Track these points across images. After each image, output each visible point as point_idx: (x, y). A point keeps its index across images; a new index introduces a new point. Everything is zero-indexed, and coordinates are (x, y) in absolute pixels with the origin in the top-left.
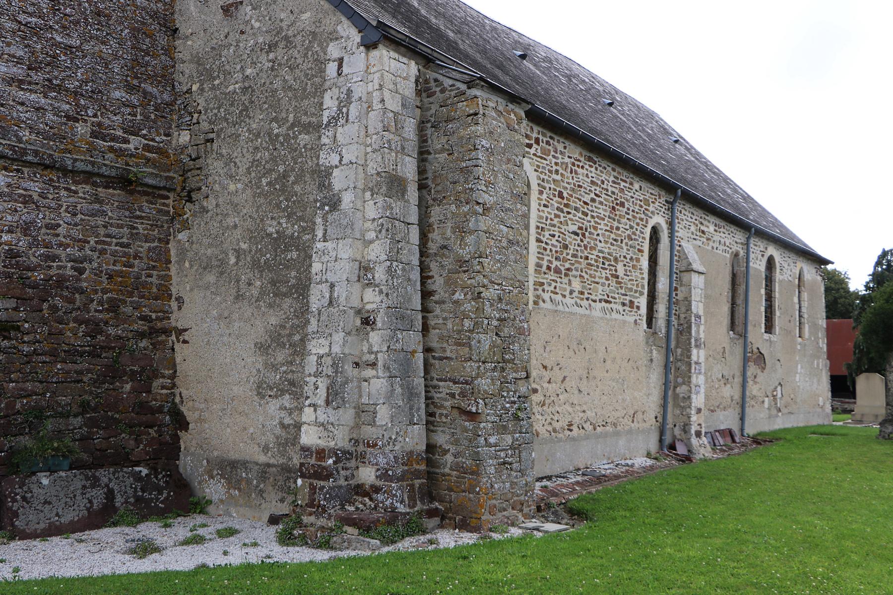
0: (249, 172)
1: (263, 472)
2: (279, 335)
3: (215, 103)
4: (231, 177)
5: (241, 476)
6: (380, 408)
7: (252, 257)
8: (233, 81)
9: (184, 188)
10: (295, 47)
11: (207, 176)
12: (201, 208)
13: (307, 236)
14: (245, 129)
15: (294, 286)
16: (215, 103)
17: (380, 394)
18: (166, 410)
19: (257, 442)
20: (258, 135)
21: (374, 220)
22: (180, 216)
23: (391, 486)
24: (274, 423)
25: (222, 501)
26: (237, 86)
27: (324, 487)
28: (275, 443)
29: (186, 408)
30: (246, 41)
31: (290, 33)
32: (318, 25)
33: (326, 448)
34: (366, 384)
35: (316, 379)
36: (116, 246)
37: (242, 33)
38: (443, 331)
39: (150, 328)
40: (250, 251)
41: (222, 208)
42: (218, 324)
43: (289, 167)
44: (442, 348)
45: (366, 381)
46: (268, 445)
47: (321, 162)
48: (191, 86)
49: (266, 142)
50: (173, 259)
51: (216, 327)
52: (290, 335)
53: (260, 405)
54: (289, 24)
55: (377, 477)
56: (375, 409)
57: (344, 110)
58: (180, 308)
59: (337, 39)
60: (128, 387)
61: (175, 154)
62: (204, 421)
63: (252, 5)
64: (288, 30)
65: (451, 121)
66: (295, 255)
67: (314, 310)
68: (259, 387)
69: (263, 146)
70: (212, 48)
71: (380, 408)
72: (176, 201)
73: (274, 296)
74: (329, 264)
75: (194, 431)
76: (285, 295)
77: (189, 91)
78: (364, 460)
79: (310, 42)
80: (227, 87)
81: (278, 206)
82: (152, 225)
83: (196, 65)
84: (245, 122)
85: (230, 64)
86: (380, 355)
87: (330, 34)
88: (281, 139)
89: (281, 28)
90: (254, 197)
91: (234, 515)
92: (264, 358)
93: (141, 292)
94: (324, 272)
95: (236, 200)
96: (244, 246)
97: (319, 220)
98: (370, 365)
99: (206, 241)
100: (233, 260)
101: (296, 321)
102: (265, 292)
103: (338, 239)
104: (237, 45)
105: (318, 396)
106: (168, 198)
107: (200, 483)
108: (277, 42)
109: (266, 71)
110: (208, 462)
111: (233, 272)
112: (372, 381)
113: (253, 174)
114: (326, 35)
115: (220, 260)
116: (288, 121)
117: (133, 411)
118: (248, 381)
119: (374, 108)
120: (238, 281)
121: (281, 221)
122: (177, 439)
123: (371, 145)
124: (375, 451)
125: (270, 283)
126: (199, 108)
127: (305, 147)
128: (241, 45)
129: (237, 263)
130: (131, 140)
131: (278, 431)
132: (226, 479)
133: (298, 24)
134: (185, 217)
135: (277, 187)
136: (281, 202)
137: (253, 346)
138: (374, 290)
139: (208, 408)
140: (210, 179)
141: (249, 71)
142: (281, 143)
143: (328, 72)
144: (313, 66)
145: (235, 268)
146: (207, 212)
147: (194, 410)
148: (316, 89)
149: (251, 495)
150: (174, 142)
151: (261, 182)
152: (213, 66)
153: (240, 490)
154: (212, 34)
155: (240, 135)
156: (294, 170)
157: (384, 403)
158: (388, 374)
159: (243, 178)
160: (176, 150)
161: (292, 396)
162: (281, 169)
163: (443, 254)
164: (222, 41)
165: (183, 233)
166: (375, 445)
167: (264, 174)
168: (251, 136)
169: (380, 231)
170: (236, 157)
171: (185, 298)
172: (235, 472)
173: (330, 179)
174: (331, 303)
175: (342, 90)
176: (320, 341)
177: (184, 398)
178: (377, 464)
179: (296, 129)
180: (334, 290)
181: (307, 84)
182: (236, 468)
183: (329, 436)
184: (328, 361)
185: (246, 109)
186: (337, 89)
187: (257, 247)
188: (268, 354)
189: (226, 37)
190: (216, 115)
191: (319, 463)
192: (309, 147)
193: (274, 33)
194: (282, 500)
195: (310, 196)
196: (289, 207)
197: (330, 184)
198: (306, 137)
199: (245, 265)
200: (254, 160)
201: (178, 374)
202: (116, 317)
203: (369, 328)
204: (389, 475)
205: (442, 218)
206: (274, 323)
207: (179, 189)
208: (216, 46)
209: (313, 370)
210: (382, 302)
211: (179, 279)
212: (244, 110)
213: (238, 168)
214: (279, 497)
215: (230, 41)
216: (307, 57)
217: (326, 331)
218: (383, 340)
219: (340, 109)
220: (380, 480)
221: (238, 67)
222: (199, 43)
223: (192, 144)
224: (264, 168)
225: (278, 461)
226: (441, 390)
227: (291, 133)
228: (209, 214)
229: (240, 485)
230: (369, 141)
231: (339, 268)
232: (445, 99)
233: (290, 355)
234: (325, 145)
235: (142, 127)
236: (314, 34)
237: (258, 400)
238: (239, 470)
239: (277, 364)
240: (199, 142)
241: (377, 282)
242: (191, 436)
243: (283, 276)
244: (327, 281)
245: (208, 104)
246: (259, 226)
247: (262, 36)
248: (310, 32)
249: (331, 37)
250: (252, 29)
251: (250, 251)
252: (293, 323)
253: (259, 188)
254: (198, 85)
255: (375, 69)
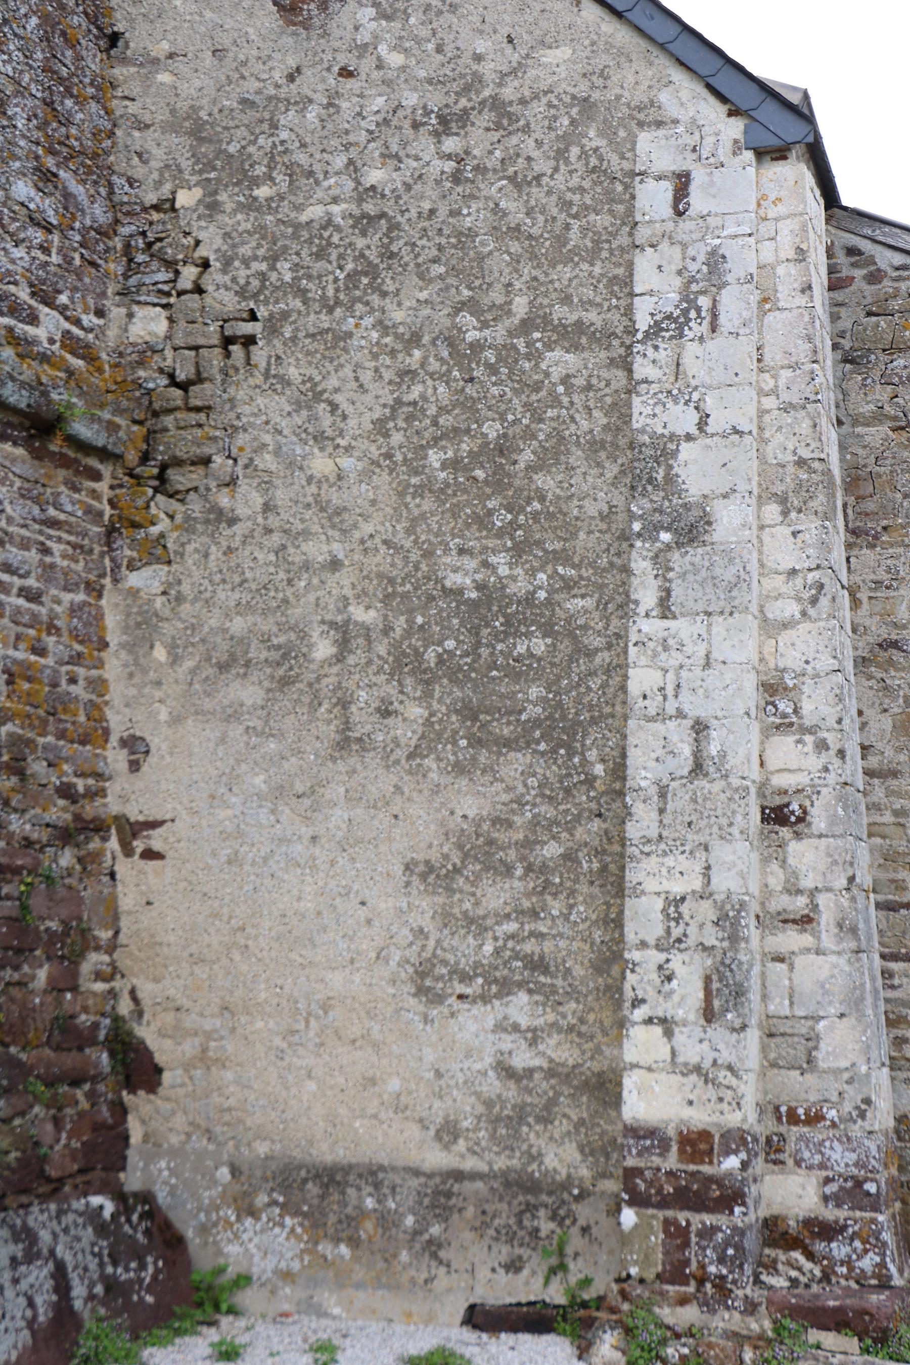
0: (381, 427)
1: (437, 1193)
2: (491, 842)
3: (259, 246)
4: (320, 438)
5: (359, 1208)
6: (831, 1028)
7: (396, 645)
8: (320, 194)
9: (145, 458)
10: (526, 129)
11: (232, 430)
12: (210, 511)
13: (580, 603)
14: (368, 321)
15: (536, 723)
16: (259, 246)
17: (826, 993)
18: (102, 1035)
19: (416, 1115)
20: (414, 340)
21: (793, 572)
22: (135, 525)
23: (873, 1221)
24: (478, 1066)
25: (287, 1276)
26: (336, 209)
27: (715, 1229)
28: (479, 1118)
29: (153, 1028)
30: (361, 96)
31: (508, 93)
32: (599, 82)
33: (713, 1130)
34: (782, 967)
35: (662, 957)
36: (19, 596)
37: (346, 73)
38: (894, 843)
39: (77, 817)
40: (387, 630)
41: (284, 516)
42: (273, 812)
43: (517, 429)
44: (893, 881)
45: (782, 960)
46: (456, 1122)
47: (637, 423)
48: (174, 193)
49: (442, 360)
50: (114, 638)
51: (264, 816)
52: (528, 844)
53: (426, 1019)
54: (505, 69)
55: (826, 1199)
56: (812, 1028)
57: (704, 302)
58: (135, 766)
59: (659, 124)
60: (42, 975)
61: (117, 365)
62: (222, 1063)
63: (376, 5)
64: (500, 85)
65: (900, 350)
66: (539, 645)
67: (643, 784)
68: (422, 975)
69: (431, 369)
70: (244, 101)
71: (831, 1028)
72: (121, 486)
73: (470, 745)
74: (684, 674)
75: (181, 1092)
76: (509, 744)
77: (168, 206)
78: (781, 1157)
79: (573, 122)
80: (299, 208)
81: (482, 521)
82: (75, 546)
83: (188, 141)
84: (367, 303)
85: (311, 149)
86: (822, 900)
87: (640, 109)
88: (490, 356)
89: (478, 78)
90: (401, 494)
91: (336, 1311)
92: (440, 900)
93: (60, 721)
94: (670, 691)
95: (335, 498)
96: (360, 614)
97: (641, 564)
98: (794, 921)
99: (226, 596)
100: (323, 649)
101: (547, 811)
102: (439, 734)
103: (709, 614)
104: (330, 105)
105: (676, 998)
106: (96, 476)
107: (204, 1230)
108: (465, 111)
109: (438, 182)
110: (235, 1171)
111: (325, 681)
112: (799, 961)
113: (397, 438)
114: (625, 110)
115: (278, 647)
116: (509, 313)
117: (48, 1043)
118: (381, 956)
119: (781, 304)
120: (344, 704)
121: (493, 560)
122: (121, 1111)
123: (775, 392)
124: (817, 1134)
125: (457, 712)
126: (202, 252)
127: (565, 380)
128: (345, 105)
129: (339, 658)
130: (42, 317)
131: (492, 1085)
132: (305, 1215)
133: (531, 73)
134: (155, 530)
135: (480, 474)
136: (490, 513)
137: (398, 870)
138: (798, 742)
139: (233, 1030)
140: (242, 439)
141: (374, 176)
142: (488, 365)
143: (642, 202)
144: (586, 184)
145: (335, 669)
146: (232, 521)
147: (177, 1033)
148: (597, 242)
149: (395, 1256)
150: (112, 333)
151: (425, 457)
152: (251, 149)
153: (354, 1242)
154: (244, 63)
155: (350, 335)
156: (534, 437)
157: (842, 1015)
158: (853, 945)
159: (362, 444)
160: (121, 355)
161: (537, 997)
162: (492, 430)
163: (890, 662)
164: (277, 86)
165: (147, 572)
166: (814, 1119)
167: (436, 440)
168: (388, 340)
169: (814, 601)
170: (337, 390)
171: (154, 742)
172: (336, 1197)
173: (671, 467)
174: (698, 768)
175: (691, 252)
176: (670, 861)
177: (146, 1002)
178: (822, 1166)
179: (536, 335)
180: (707, 737)
181: (567, 227)
182: (341, 1186)
183: (721, 1100)
184: (706, 911)
185: (372, 271)
186: (677, 249)
187: (411, 622)
188: (450, 891)
189: (291, 78)
190: (263, 277)
191: (692, 1167)
192: (579, 382)
193: (455, 87)
194: (514, 1266)
195: (586, 503)
196: (520, 527)
197: (670, 479)
198: (570, 357)
199: (369, 662)
200: (399, 402)
201: (122, 939)
202: (22, 788)
203: (785, 832)
204: (868, 1194)
205: (882, 575)
206: (471, 814)
207: (132, 457)
208: (257, 98)
209: (655, 930)
210: (826, 770)
211: (132, 691)
212: (366, 274)
213: (344, 417)
214: (503, 1258)
215: (307, 91)
216: (567, 162)
217: (690, 837)
218: (835, 862)
219: (688, 299)
220: (838, 1206)
221: (340, 161)
222: (198, 83)
223: (179, 342)
224: (435, 423)
225: (490, 1164)
226: (896, 982)
227: (521, 343)
228: (239, 529)
229: (357, 1229)
230: (768, 382)
231: (720, 685)
232: (882, 297)
233: (528, 895)
234: (646, 381)
235: (60, 285)
236: (586, 104)
237: (421, 1008)
238: (351, 1191)
239: (484, 917)
240: (201, 341)
241: (807, 722)
242: (168, 1106)
243: (502, 696)
244: (680, 714)
245: (234, 246)
246: (417, 568)
247: (415, 89)
248: (574, 97)
249: (641, 116)
250: (379, 67)
251: (387, 630)
252: (534, 816)
253: (416, 473)
254: (198, 193)
255: (781, 209)
